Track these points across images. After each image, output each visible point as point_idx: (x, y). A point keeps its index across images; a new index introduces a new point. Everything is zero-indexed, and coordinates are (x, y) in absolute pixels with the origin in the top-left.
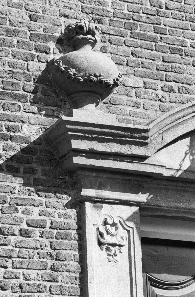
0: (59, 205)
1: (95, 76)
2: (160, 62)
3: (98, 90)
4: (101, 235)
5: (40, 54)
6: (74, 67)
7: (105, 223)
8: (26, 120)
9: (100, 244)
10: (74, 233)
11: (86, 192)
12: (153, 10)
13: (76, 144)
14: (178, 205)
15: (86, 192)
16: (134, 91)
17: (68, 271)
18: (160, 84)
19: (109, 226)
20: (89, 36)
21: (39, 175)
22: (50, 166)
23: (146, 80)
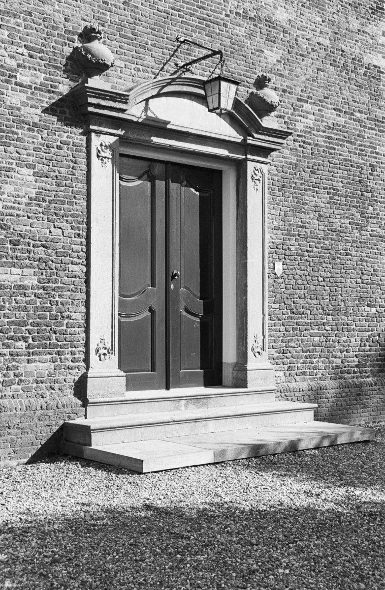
0: (77, 133)
1: (102, 60)
2: (134, 53)
3: (100, 67)
4: (99, 151)
6: (90, 53)
8: (61, 82)
9: (98, 156)
11: (92, 127)
12: (132, 21)
13: (90, 100)
14: (140, 138)
15: (92, 127)
16: (119, 69)
17: (81, 170)
18: (134, 66)
19: (103, 147)
20: (98, 35)
22: (74, 110)
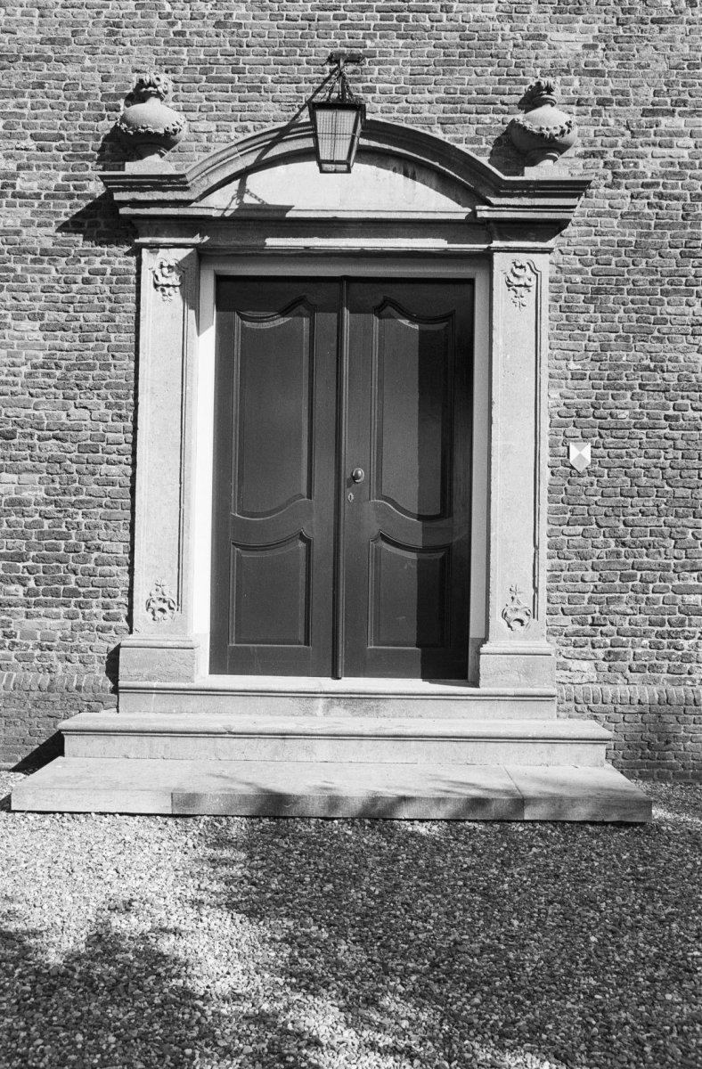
1: (143, 128)
2: (237, 103)
5: (109, 113)
7: (162, 267)
9: (156, 286)
10: (133, 278)
17: (125, 312)
18: (234, 125)
20: (151, 89)
21: (102, 228)
22: (105, 222)
23: (219, 123)
